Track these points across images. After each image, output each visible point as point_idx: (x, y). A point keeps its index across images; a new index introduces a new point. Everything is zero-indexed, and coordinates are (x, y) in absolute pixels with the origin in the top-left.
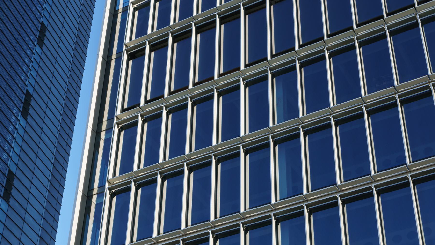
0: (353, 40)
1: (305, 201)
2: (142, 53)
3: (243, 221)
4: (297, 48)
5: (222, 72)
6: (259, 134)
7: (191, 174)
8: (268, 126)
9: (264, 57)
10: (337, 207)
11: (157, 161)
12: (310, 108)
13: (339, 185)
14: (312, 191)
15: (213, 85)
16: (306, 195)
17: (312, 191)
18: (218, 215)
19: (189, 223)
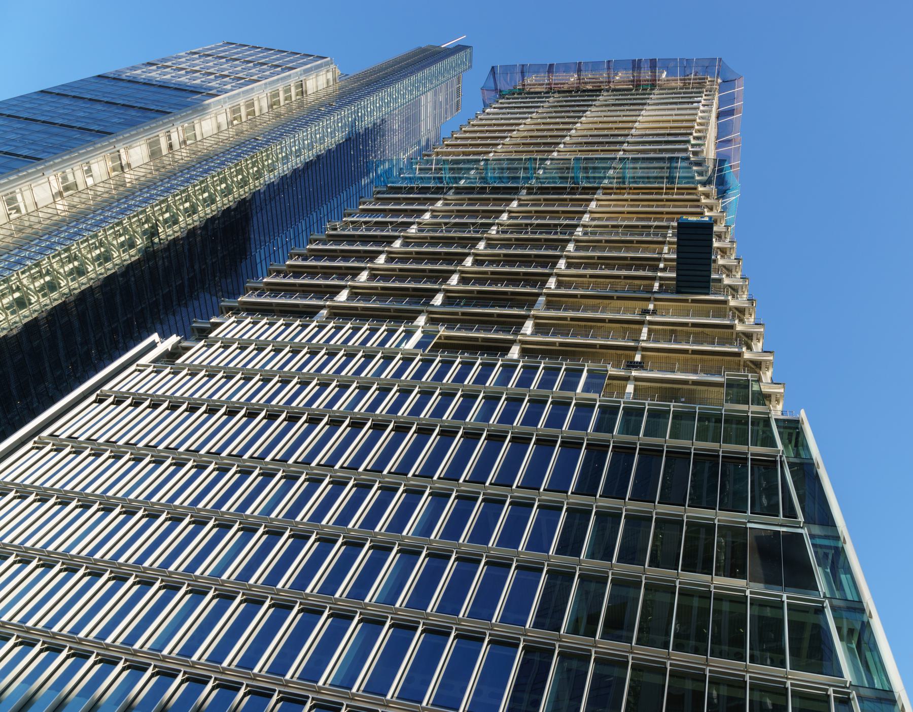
0: (563, 503)
1: (456, 624)
2: (406, 430)
3: (457, 626)
4: (514, 487)
5: (467, 479)
6: (447, 544)
7: (98, 513)
8: (487, 545)
9: (406, 473)
10: (413, 632)
11: (401, 532)
12: (501, 542)
13: (494, 624)
14: (467, 617)
15: (429, 483)
16: (460, 618)
17: (467, 617)
18: (374, 600)
19: (404, 605)
